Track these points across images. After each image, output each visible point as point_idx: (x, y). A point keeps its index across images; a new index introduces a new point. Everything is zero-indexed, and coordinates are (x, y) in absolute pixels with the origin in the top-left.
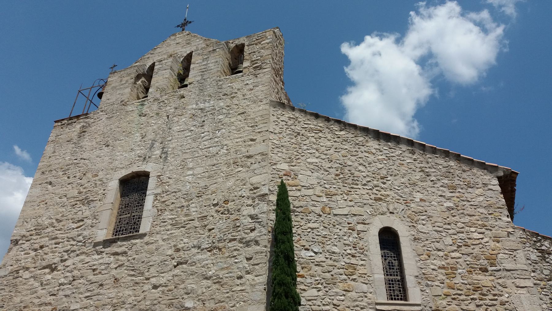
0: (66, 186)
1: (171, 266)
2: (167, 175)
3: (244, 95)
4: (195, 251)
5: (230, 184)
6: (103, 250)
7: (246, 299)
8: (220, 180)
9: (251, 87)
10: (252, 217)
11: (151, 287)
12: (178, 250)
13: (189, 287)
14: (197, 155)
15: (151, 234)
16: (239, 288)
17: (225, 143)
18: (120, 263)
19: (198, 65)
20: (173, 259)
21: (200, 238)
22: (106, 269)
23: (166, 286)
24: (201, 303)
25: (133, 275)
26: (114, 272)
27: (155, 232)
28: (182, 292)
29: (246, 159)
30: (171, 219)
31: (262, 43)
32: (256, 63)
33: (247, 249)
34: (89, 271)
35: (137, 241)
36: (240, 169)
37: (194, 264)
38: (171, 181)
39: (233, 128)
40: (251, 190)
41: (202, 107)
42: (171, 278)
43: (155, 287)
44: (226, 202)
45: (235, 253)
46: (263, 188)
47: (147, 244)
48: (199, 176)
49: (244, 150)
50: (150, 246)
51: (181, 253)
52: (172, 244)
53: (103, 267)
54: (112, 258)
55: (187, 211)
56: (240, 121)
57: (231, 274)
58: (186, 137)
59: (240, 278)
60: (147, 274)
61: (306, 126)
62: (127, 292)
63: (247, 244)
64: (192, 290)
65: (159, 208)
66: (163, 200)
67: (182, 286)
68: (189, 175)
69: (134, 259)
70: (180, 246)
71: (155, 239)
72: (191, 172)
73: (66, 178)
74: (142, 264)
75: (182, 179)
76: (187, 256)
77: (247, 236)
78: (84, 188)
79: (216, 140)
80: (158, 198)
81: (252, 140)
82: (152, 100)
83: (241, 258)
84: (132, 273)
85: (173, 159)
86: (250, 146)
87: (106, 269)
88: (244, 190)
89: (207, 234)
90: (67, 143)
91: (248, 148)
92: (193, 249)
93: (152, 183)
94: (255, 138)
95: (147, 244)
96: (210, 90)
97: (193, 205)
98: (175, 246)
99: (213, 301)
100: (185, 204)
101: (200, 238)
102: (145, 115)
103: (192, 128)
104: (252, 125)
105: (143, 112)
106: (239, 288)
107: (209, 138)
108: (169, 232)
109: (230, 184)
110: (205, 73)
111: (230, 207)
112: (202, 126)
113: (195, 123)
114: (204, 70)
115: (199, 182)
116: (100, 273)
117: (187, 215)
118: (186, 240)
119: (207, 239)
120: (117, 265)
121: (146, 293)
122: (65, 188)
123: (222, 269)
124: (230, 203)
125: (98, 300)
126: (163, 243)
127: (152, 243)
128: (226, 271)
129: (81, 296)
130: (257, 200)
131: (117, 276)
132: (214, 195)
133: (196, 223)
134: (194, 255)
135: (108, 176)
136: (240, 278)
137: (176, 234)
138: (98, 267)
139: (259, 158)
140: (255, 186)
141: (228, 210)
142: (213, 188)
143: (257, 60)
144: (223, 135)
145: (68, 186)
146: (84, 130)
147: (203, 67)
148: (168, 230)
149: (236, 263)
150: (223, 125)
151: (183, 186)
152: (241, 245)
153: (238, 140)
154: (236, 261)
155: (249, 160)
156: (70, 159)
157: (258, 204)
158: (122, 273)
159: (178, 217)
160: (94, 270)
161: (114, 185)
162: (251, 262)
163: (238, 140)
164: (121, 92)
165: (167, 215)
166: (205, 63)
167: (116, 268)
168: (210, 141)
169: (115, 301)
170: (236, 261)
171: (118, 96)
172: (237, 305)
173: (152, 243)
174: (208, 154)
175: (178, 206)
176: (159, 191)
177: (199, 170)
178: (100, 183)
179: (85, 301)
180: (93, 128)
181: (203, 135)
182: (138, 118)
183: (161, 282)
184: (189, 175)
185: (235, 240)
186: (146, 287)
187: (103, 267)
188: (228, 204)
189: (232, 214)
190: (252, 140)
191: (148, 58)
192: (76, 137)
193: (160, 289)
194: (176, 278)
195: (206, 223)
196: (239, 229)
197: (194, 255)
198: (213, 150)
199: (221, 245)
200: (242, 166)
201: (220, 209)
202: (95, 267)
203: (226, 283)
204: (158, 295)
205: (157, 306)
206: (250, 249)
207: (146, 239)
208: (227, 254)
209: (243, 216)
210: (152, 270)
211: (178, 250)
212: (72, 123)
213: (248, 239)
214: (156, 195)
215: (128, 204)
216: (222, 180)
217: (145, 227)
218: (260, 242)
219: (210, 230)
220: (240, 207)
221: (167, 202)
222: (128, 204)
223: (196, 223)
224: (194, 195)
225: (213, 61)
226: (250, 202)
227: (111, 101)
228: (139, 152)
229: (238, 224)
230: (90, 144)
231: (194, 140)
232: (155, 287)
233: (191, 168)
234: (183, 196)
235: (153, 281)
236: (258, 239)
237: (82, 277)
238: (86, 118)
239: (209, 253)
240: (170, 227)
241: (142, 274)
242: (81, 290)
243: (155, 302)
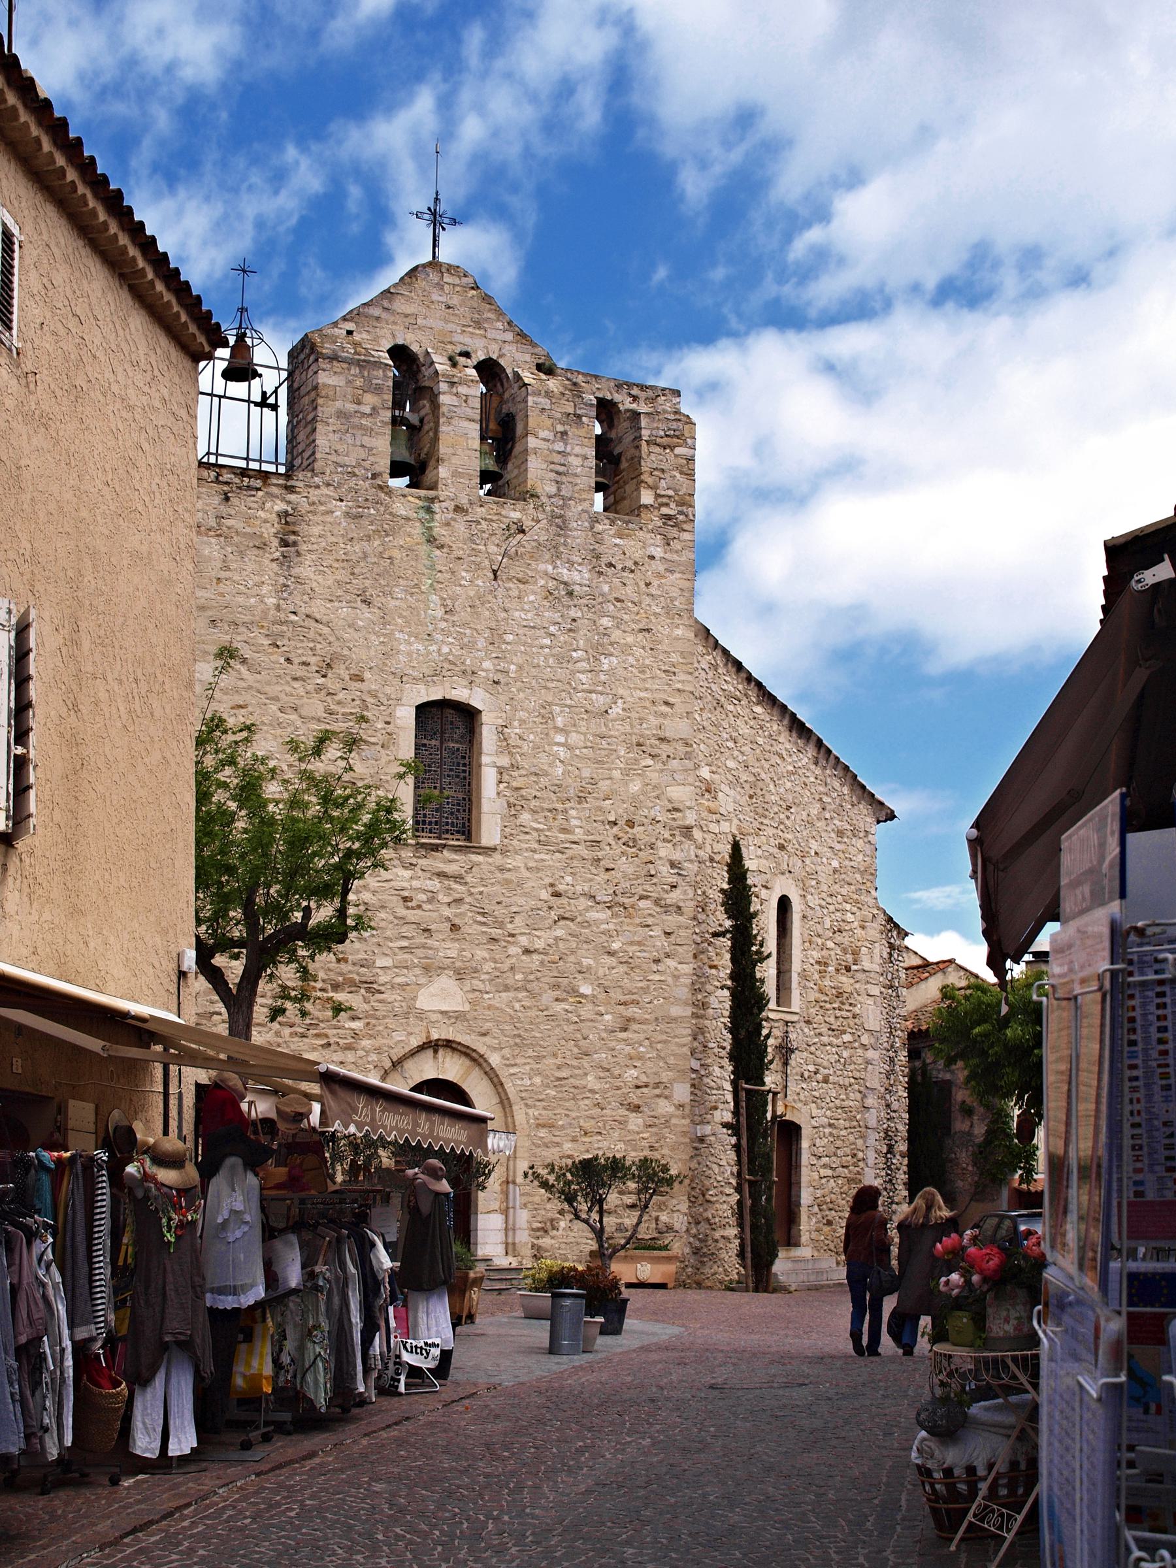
0: (288, 683)
1: (550, 921)
2: (517, 731)
3: (648, 585)
4: (584, 903)
5: (635, 787)
6: (414, 861)
7: (666, 995)
8: (616, 774)
9: (661, 568)
10: (673, 865)
11: (520, 951)
12: (557, 895)
13: (585, 962)
14: (568, 702)
15: (504, 852)
16: (657, 977)
17: (621, 691)
18: (458, 896)
19: (543, 445)
20: (550, 908)
21: (591, 880)
22: (429, 901)
23: (546, 954)
24: (602, 990)
25: (484, 924)
26: (447, 912)
27: (510, 848)
28: (573, 968)
29: (657, 742)
30: (537, 830)
31: (678, 451)
32: (667, 505)
33: (664, 917)
34: (394, 898)
35: (480, 858)
36: (650, 762)
37: (587, 924)
38: (526, 747)
39: (631, 660)
40: (669, 811)
41: (566, 579)
42: (551, 941)
43: (527, 951)
44: (631, 824)
45: (650, 921)
46: (688, 812)
47: (501, 869)
48: (577, 752)
49: (654, 721)
50: (507, 875)
51: (564, 900)
52: (548, 881)
53: (423, 897)
54: (435, 884)
55: (564, 822)
56: (643, 648)
57: (645, 954)
58: (542, 648)
59: (657, 961)
60: (509, 926)
61: (725, 687)
62: (481, 953)
63: (666, 909)
64: (589, 968)
65: (512, 800)
66: (515, 784)
67: (572, 959)
68: (559, 744)
69: (481, 893)
70: (561, 888)
71: (514, 864)
72: (563, 740)
73: (282, 660)
74: (499, 907)
75: (547, 748)
76: (573, 908)
77: (666, 896)
78: (339, 703)
79: (603, 677)
80: (506, 777)
81: (666, 703)
82: (450, 505)
83: (657, 932)
84: (480, 918)
85: (522, 695)
86: (664, 715)
87: (429, 901)
88: (658, 808)
89: (605, 876)
90: (256, 551)
91: (661, 720)
92: (582, 899)
93: (488, 737)
94: (671, 700)
95: (501, 869)
96: (578, 535)
97: (573, 813)
98: (552, 885)
99: (619, 990)
100: (559, 806)
101: (591, 880)
102: (442, 546)
103: (552, 629)
104: (667, 668)
105: (436, 532)
106: (657, 977)
107: (588, 668)
108: (537, 856)
109: (635, 787)
110: (564, 479)
111: (638, 836)
112: (570, 630)
113: (557, 617)
114: (561, 469)
115: (579, 765)
116: (419, 907)
117: (564, 830)
118: (569, 879)
119: (605, 886)
120: (449, 899)
121: (514, 960)
122: (288, 689)
123: (631, 943)
124: (637, 829)
125: (426, 958)
126: (528, 874)
127: (509, 870)
128: (637, 948)
129: (391, 944)
130: (677, 833)
131: (457, 921)
132: (607, 802)
133: (581, 850)
134: (587, 910)
135: (388, 690)
136: (657, 961)
137: (551, 863)
138: (413, 894)
139: (681, 749)
140: (676, 805)
141: (634, 840)
142: (604, 785)
143: (670, 497)
144: (611, 672)
145: (296, 684)
146: (291, 528)
147: (558, 458)
148: (534, 851)
149: (651, 936)
150: (611, 644)
151: (550, 765)
152: (658, 909)
153: (643, 694)
154: (651, 933)
155: (664, 746)
156: (278, 608)
157: (681, 842)
158: (466, 916)
159: (549, 830)
160: (405, 899)
161: (406, 717)
162: (672, 938)
163: (643, 694)
164: (366, 441)
165: (525, 817)
166: (559, 446)
167: (449, 904)
168: (589, 675)
169: (458, 964)
170: (651, 933)
171: (363, 454)
172: (655, 1002)
173: (509, 870)
174: (589, 708)
175: (546, 806)
176: (504, 761)
177: (574, 738)
178: (372, 701)
179: (402, 956)
180: (316, 530)
181: (574, 654)
182: (425, 548)
183: (537, 946)
184: (559, 744)
185: (647, 897)
186: (513, 950)
187: (423, 897)
188: (633, 827)
189: (640, 850)
190: (666, 703)
191: (378, 318)
192: (275, 543)
193: (535, 957)
194: (561, 944)
195: (600, 854)
196: (655, 880)
197: (587, 910)
198: (600, 701)
199: (626, 901)
200: (653, 756)
201: (621, 835)
202: (406, 894)
203: (638, 967)
204: (534, 967)
205: (534, 984)
206: (670, 918)
207: (497, 858)
208: (638, 921)
209: (660, 858)
210: (518, 920)
211: (557, 895)
212: (249, 488)
213: (669, 902)
214: (501, 771)
215: (430, 766)
216: (620, 776)
217: (490, 831)
218: (684, 910)
219: (607, 870)
220: (653, 840)
221: (523, 792)
222: (430, 766)
223: (581, 850)
224: (571, 793)
225: (577, 450)
226: (667, 835)
227: (346, 460)
228: (445, 649)
229: (653, 872)
230: (320, 578)
231: (559, 659)
232: (527, 951)
233: (562, 730)
234: (553, 788)
235: (524, 941)
236: (681, 904)
237: (383, 907)
238: (286, 487)
239: (609, 913)
240: (536, 846)
241: (501, 926)
242: (388, 933)
243: (532, 977)
